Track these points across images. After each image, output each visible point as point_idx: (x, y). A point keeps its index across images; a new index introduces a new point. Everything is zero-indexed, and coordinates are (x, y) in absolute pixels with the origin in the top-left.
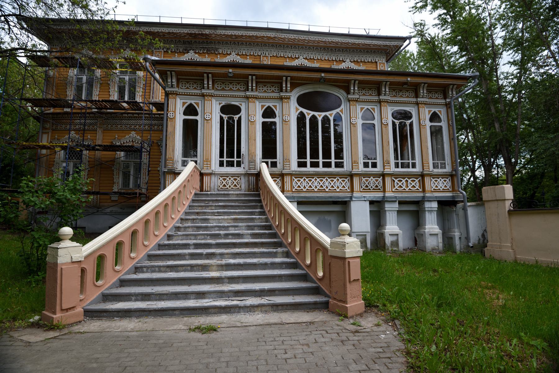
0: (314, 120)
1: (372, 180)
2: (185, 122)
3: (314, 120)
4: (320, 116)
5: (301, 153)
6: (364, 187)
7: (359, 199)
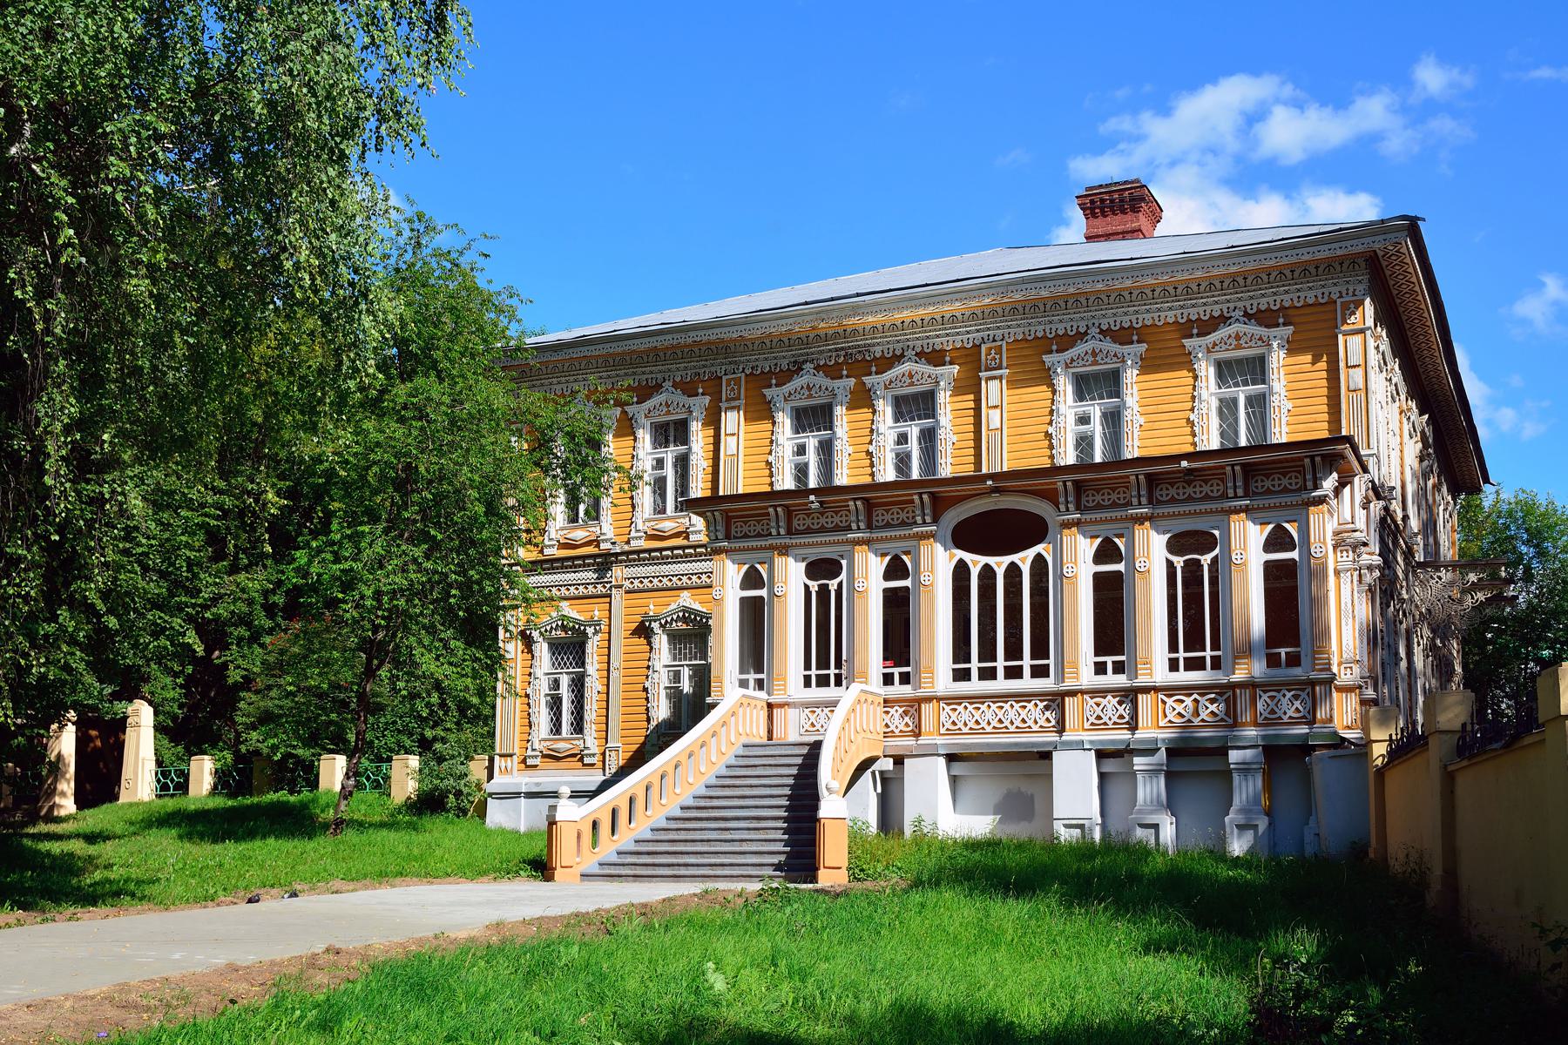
0: (988, 573)
1: (1111, 701)
2: (1099, 579)
3: (988, 573)
4: (1000, 564)
5: (961, 651)
6: (1092, 720)
7: (1079, 746)
